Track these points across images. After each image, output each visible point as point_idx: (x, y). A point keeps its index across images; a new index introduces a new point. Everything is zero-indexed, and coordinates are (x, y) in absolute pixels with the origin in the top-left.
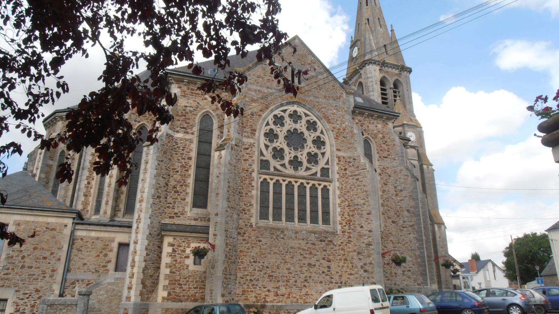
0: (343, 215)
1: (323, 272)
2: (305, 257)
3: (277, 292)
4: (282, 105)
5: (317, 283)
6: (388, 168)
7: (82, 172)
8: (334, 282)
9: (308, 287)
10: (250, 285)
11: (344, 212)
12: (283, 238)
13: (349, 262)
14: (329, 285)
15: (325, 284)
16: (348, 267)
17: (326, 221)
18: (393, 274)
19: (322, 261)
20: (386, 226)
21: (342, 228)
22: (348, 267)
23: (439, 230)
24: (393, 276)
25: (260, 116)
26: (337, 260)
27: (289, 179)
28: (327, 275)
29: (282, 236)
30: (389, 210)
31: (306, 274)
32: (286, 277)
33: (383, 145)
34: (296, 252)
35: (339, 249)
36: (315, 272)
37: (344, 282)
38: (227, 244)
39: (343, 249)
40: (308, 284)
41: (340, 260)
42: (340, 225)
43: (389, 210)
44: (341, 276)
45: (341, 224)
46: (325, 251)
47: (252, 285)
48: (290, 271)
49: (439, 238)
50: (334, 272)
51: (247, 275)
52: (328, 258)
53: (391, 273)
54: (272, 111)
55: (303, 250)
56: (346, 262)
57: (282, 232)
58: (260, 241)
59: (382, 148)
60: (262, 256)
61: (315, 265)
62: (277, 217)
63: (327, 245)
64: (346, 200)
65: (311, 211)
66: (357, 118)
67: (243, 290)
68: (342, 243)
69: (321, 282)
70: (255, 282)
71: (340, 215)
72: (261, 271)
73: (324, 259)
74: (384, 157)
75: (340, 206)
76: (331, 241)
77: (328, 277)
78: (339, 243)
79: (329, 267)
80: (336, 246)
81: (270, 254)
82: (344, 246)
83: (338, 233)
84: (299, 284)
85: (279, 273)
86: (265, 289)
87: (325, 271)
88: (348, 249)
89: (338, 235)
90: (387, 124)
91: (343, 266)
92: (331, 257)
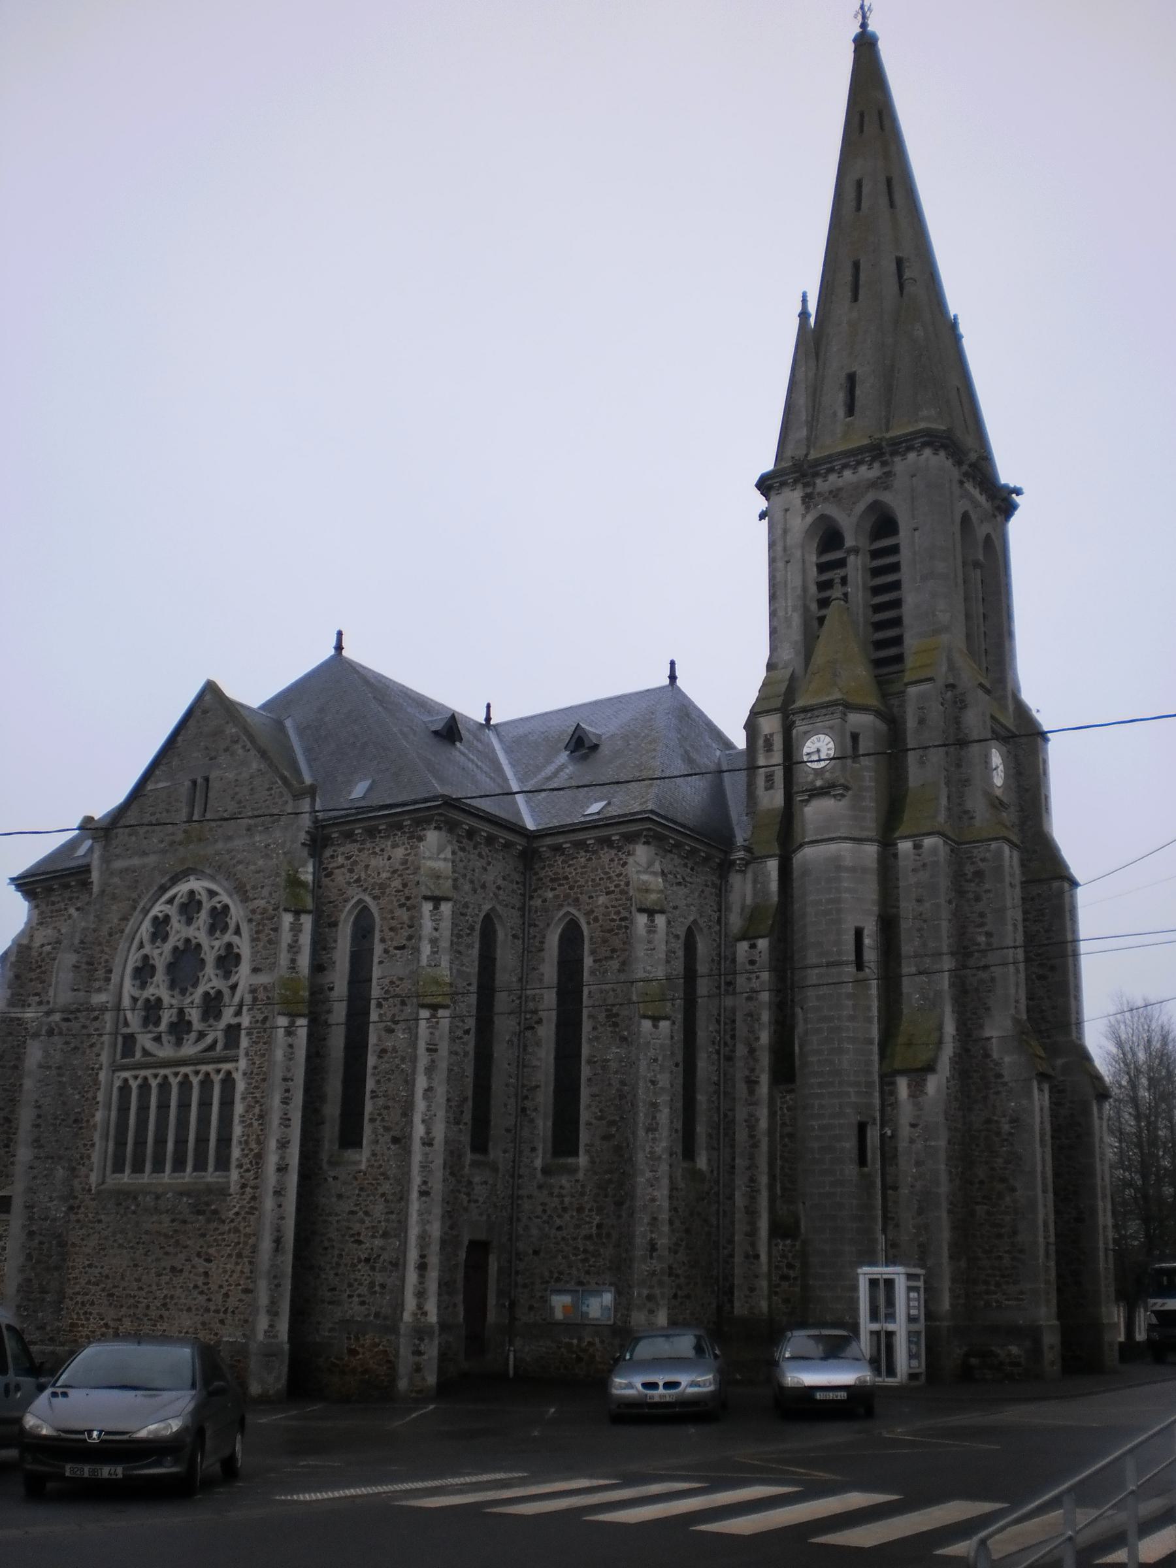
0: (246, 1142)
1: (196, 1287)
2: (167, 1253)
3: (118, 1329)
4: (163, 889)
5: (182, 1310)
6: (401, 979)
7: (726, 915)
8: (213, 1308)
9: (166, 1320)
10: (81, 1312)
11: (248, 1136)
12: (134, 1212)
13: (246, 1260)
14: (202, 1315)
15: (197, 1314)
16: (242, 1272)
17: (223, 1163)
18: (377, 1288)
19: (196, 1260)
20: (374, 1154)
21: (242, 1177)
22: (242, 1272)
23: (912, 1095)
24: (375, 1292)
25: (122, 931)
26: (222, 1257)
27: (162, 1072)
28: (202, 1293)
29: (133, 1208)
30: (387, 1108)
31: (165, 1292)
32: (135, 1296)
33: (399, 912)
34: (153, 1242)
35: (230, 1230)
36: (181, 1287)
37: (230, 1310)
38: (31, 1234)
39: (237, 1230)
40: (167, 1312)
41: (230, 1256)
42: (238, 1170)
43: (387, 1108)
44: (226, 1295)
45: (240, 1166)
46: (203, 1235)
47: (83, 1314)
48: (140, 1284)
49: (913, 1126)
50: (214, 1287)
51: (78, 1293)
52: (207, 1254)
53: (372, 1285)
54: (146, 912)
55: (166, 1236)
56: (240, 1260)
57: (135, 1198)
58: (100, 1221)
59: (394, 923)
60: (102, 1253)
61: (181, 1271)
62: (138, 1168)
63: (209, 1221)
64: (257, 1102)
65: (219, 1141)
66: (342, 849)
67: (71, 1323)
68: (237, 1214)
69: (189, 1310)
70: (87, 1308)
71: (240, 1142)
72: (98, 1285)
73: (199, 1255)
74: (397, 948)
75: (243, 1122)
76: (215, 1212)
77: (202, 1298)
78: (231, 1214)
79: (206, 1274)
80: (224, 1222)
81: (113, 1247)
82: (239, 1223)
83: (232, 1190)
84: (153, 1314)
85: (124, 1289)
86: (102, 1322)
87: (200, 1283)
88: (248, 1230)
89: (230, 1195)
90: (420, 839)
91: (233, 1272)
92: (212, 1251)
